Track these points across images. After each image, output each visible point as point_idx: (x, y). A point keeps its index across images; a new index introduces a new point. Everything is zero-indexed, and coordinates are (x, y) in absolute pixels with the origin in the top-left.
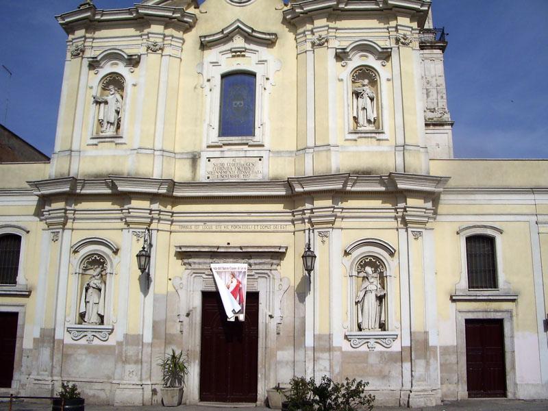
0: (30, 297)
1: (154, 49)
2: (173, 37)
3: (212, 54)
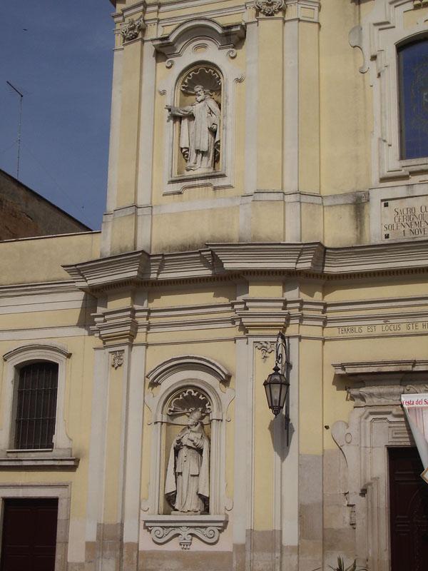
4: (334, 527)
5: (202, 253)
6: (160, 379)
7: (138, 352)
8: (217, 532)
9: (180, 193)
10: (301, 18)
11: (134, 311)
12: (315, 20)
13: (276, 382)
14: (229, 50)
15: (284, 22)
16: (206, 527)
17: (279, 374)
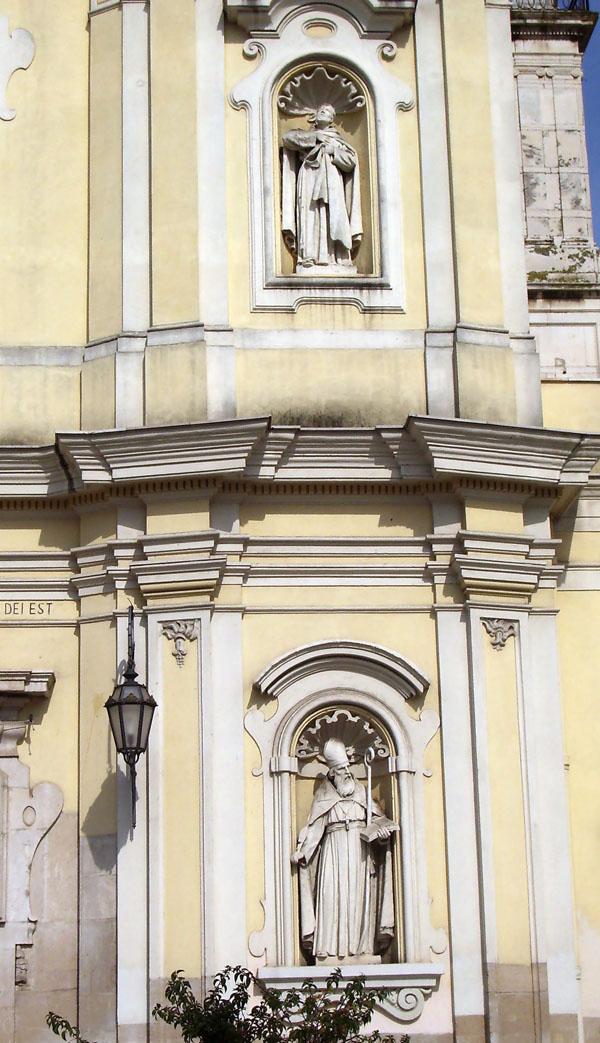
5: (384, 435)
6: (276, 689)
7: (218, 630)
8: (420, 997)
9: (290, 311)
11: (218, 540)
13: (131, 702)
16: (398, 990)
17: (136, 684)
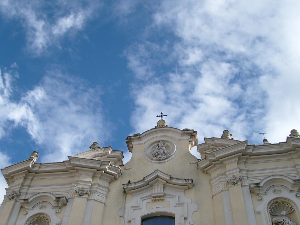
0: (192, 178)
1: (81, 193)
2: (99, 185)
3: (133, 201)
4: (158, 86)
10: (96, 199)
12: (104, 202)
14: (57, 209)
15: (88, 200)
